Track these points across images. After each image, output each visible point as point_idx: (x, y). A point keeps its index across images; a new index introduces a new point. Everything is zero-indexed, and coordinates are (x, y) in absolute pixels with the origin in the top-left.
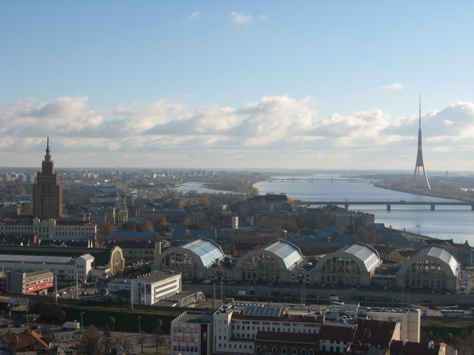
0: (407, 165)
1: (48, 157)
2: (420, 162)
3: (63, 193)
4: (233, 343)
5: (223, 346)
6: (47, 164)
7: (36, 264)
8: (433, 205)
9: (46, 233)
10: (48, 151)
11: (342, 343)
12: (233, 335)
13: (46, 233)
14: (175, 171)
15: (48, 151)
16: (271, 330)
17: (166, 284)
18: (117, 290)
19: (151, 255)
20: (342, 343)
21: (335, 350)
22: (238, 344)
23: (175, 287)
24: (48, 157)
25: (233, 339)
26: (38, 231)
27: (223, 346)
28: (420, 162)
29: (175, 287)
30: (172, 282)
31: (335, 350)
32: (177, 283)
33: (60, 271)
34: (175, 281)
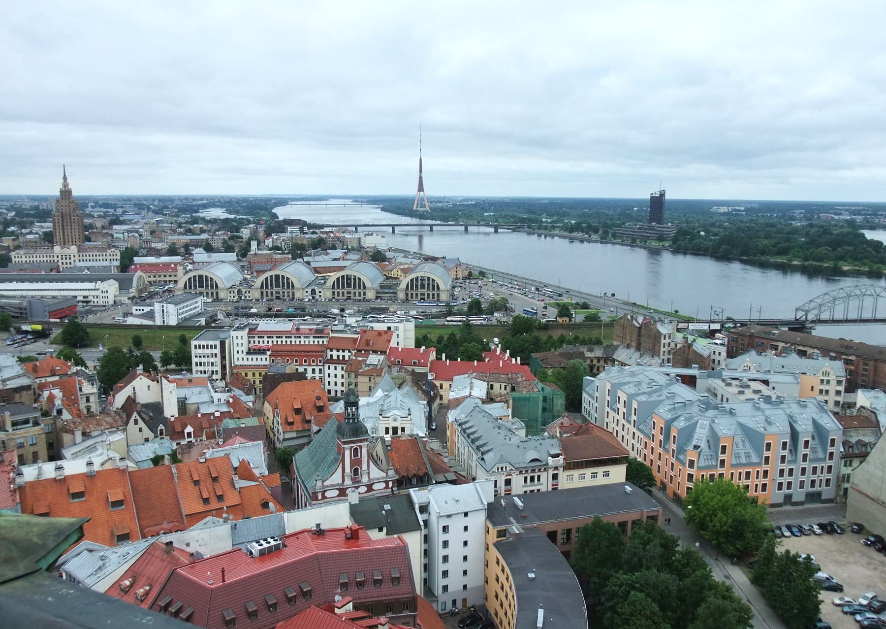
0: (411, 191)
1: (65, 185)
2: (421, 188)
3: (606, 243)
4: (250, 357)
5: (241, 359)
6: (66, 193)
7: (366, 291)
8: (431, 226)
9: (68, 261)
10: (65, 178)
11: (347, 352)
12: (249, 349)
13: (68, 261)
14: (266, 203)
15: (65, 178)
16: (302, 343)
17: (187, 306)
18: (141, 312)
19: (175, 279)
20: (347, 352)
21: (341, 358)
22: (254, 357)
23: (197, 307)
24: (65, 185)
25: (249, 353)
26: (59, 259)
27: (241, 359)
28: (421, 188)
29: (197, 307)
30: (193, 304)
31: (341, 358)
32: (199, 304)
33: (84, 297)
34: (197, 302)
